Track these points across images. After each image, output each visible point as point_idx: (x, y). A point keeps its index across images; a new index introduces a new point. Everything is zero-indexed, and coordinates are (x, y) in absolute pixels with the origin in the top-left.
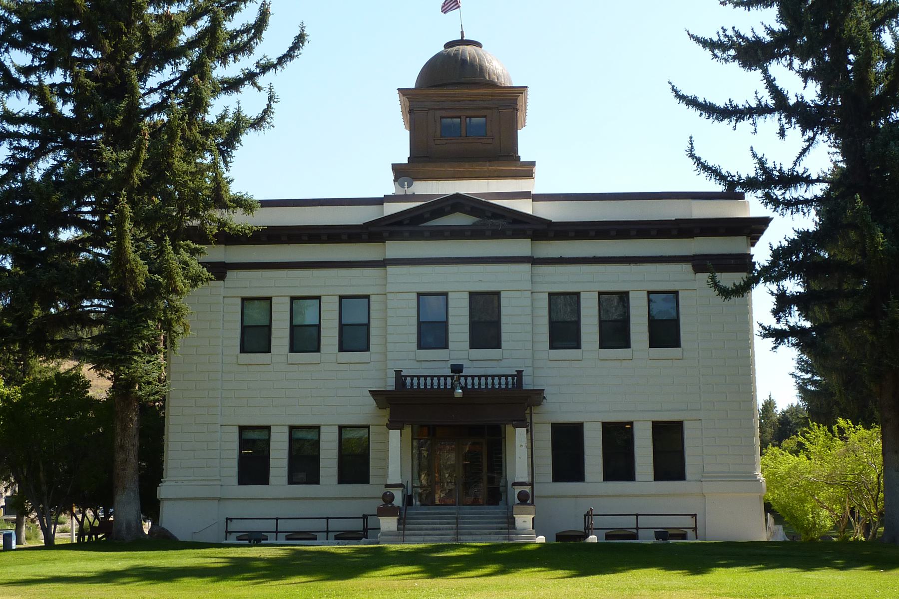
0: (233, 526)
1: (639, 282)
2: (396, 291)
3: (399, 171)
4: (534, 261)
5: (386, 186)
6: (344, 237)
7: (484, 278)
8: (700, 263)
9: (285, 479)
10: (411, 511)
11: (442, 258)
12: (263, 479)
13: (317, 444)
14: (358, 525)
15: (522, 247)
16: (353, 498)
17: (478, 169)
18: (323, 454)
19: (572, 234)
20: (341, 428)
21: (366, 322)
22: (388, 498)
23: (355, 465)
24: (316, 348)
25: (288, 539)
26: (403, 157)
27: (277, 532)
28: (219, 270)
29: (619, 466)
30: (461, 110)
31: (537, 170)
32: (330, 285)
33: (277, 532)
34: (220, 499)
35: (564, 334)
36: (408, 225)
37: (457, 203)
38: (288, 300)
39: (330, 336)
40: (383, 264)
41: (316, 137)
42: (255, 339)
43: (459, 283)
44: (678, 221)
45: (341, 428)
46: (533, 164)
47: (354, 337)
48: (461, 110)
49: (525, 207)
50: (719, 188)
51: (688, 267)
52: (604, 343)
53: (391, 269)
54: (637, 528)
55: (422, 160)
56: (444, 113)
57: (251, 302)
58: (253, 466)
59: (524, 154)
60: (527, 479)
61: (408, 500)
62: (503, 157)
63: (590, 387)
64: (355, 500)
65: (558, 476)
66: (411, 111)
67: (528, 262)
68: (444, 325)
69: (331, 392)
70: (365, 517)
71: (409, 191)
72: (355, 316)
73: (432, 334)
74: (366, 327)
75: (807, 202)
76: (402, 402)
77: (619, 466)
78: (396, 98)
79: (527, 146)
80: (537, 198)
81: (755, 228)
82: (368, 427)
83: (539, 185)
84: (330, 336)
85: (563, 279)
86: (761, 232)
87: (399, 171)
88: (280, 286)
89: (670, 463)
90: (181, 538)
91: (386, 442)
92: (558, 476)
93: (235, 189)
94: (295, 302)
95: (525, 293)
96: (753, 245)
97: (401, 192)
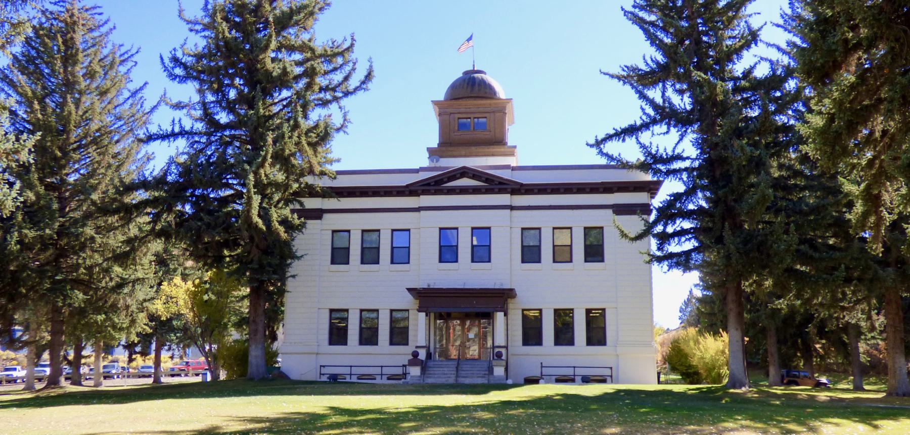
0: (324, 371)
1: (581, 220)
2: (424, 225)
3: (432, 152)
4: (512, 208)
5: (425, 162)
6: (395, 193)
9: (357, 342)
10: (431, 363)
13: (346, 320)
14: (399, 371)
15: (504, 199)
17: (480, 150)
19: (588, 190)
20: (392, 311)
22: (415, 355)
23: (399, 335)
25: (359, 379)
26: (434, 142)
27: (351, 375)
28: (317, 214)
30: (471, 112)
31: (517, 151)
32: (385, 223)
33: (351, 375)
35: (531, 254)
37: (464, 172)
38: (330, 232)
39: (547, 252)
40: (512, 208)
41: (381, 131)
42: (340, 256)
43: (581, 220)
45: (392, 311)
46: (515, 147)
47: (401, 255)
48: (471, 112)
49: (506, 175)
50: (603, 161)
51: (610, 211)
55: (448, 144)
56: (461, 116)
57: (370, 233)
58: (338, 335)
59: (510, 141)
60: (503, 344)
61: (429, 356)
62: (496, 141)
63: (545, 288)
64: (402, 354)
65: (526, 341)
66: (440, 115)
68: (347, 250)
69: (381, 289)
70: (404, 366)
71: (438, 165)
72: (400, 241)
75: (679, 171)
78: (431, 106)
79: (512, 137)
80: (514, 169)
81: (652, 188)
82: (408, 310)
83: (512, 161)
84: (464, 252)
86: (658, 189)
87: (432, 152)
88: (356, 224)
89: (597, 334)
90: (294, 376)
91: (417, 320)
92: (526, 341)
95: (506, 226)
96: (653, 197)
97: (433, 165)
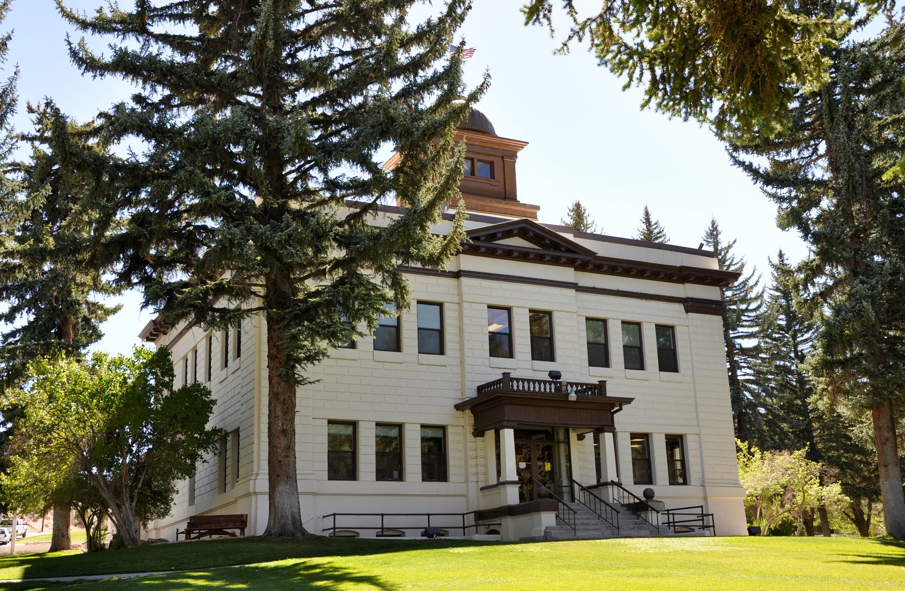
1: (650, 315)
7: (543, 298)
8: (693, 306)
11: (536, 279)
12: (352, 475)
15: (566, 274)
16: (438, 495)
18: (299, 447)
21: (438, 327)
24: (592, 363)
29: (390, 465)
34: (314, 494)
36: (483, 241)
39: (410, 338)
43: (524, 300)
44: (682, 268)
47: (434, 341)
51: (680, 307)
52: (662, 368)
53: (464, 280)
54: (476, 526)
67: (573, 288)
73: (501, 345)
74: (437, 334)
76: (489, 407)
77: (390, 465)
85: (600, 306)
93: (570, 221)
94: (438, 308)
